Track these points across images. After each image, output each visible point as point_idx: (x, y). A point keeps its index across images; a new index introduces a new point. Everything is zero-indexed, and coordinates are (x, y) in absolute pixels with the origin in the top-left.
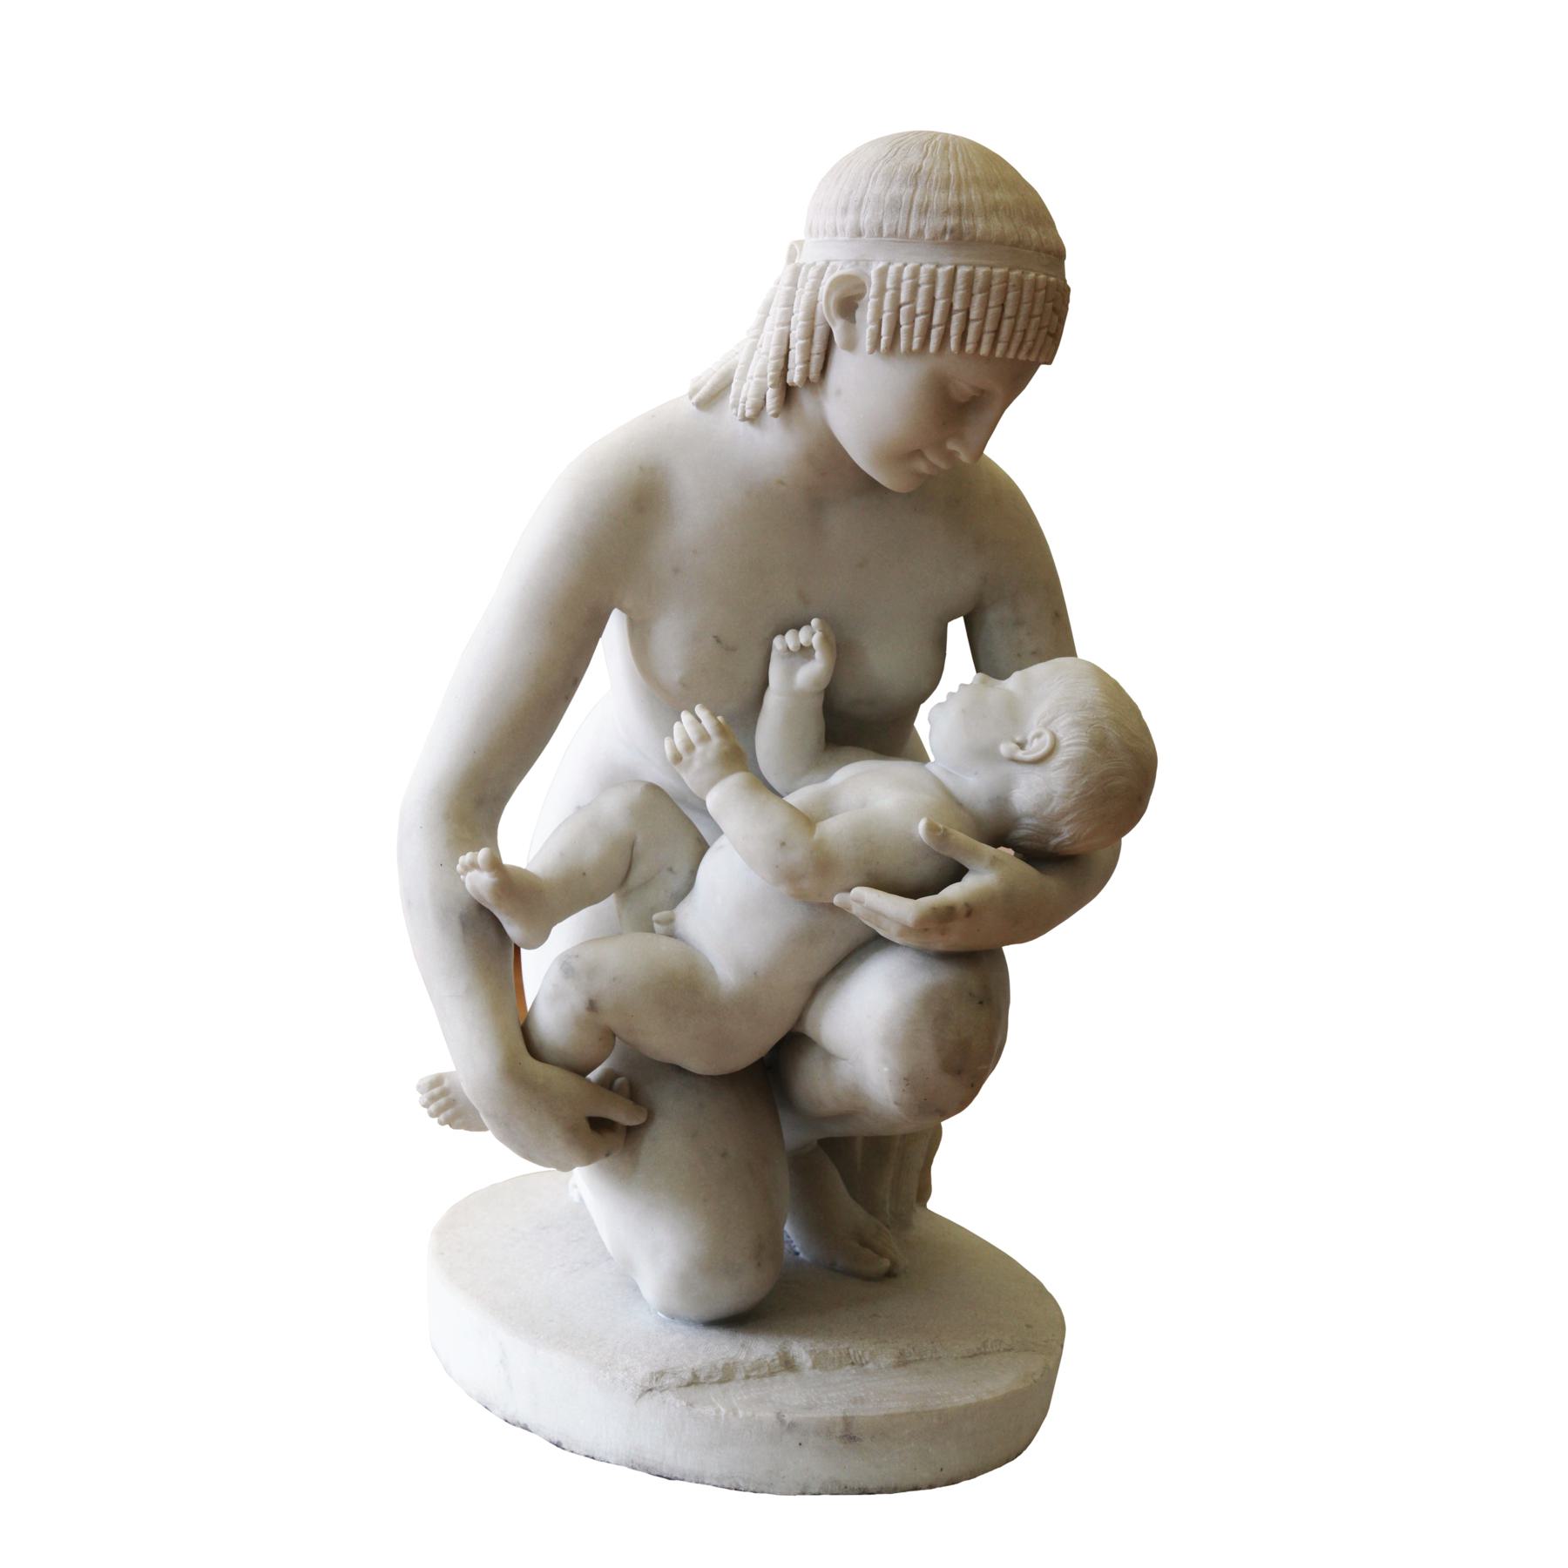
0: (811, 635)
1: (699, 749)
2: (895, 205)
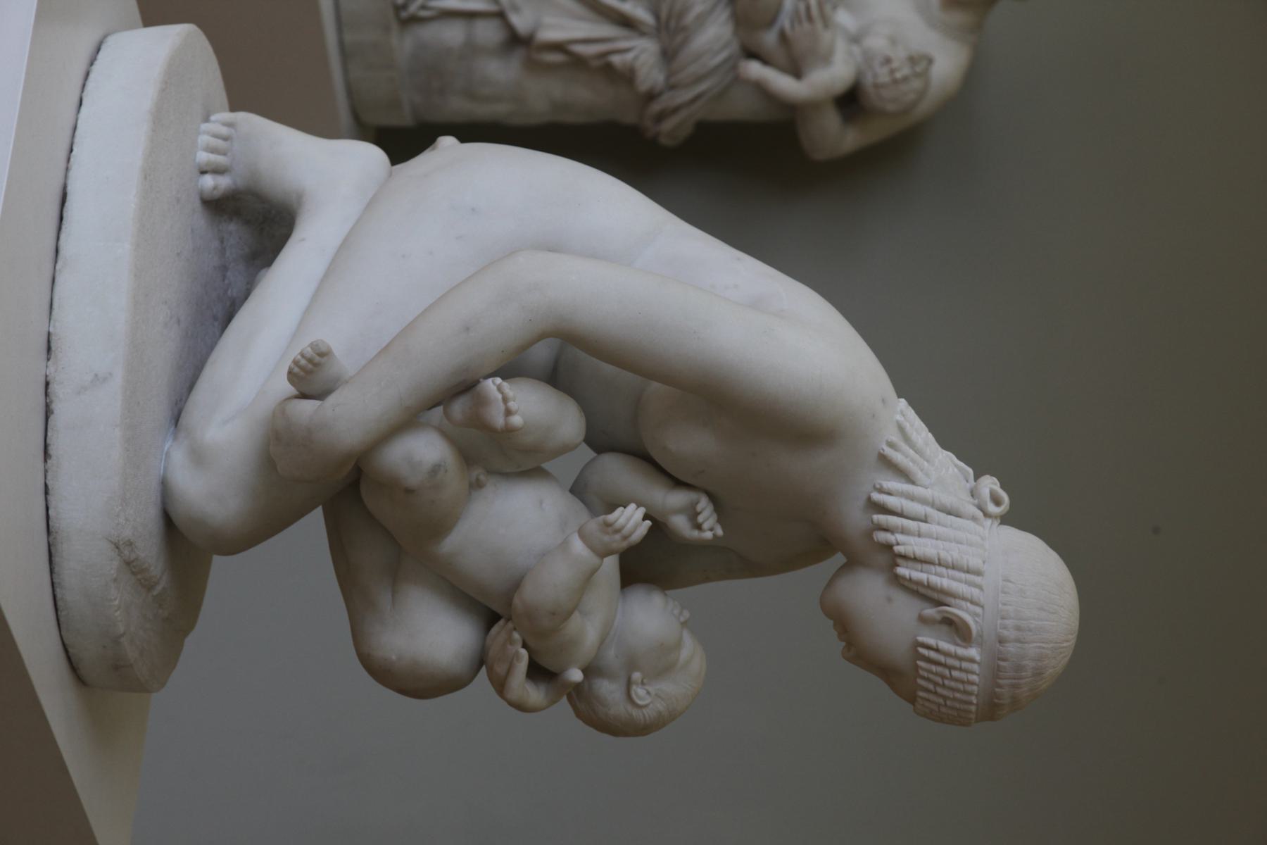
0: (710, 528)
1: (617, 537)
2: (1019, 668)
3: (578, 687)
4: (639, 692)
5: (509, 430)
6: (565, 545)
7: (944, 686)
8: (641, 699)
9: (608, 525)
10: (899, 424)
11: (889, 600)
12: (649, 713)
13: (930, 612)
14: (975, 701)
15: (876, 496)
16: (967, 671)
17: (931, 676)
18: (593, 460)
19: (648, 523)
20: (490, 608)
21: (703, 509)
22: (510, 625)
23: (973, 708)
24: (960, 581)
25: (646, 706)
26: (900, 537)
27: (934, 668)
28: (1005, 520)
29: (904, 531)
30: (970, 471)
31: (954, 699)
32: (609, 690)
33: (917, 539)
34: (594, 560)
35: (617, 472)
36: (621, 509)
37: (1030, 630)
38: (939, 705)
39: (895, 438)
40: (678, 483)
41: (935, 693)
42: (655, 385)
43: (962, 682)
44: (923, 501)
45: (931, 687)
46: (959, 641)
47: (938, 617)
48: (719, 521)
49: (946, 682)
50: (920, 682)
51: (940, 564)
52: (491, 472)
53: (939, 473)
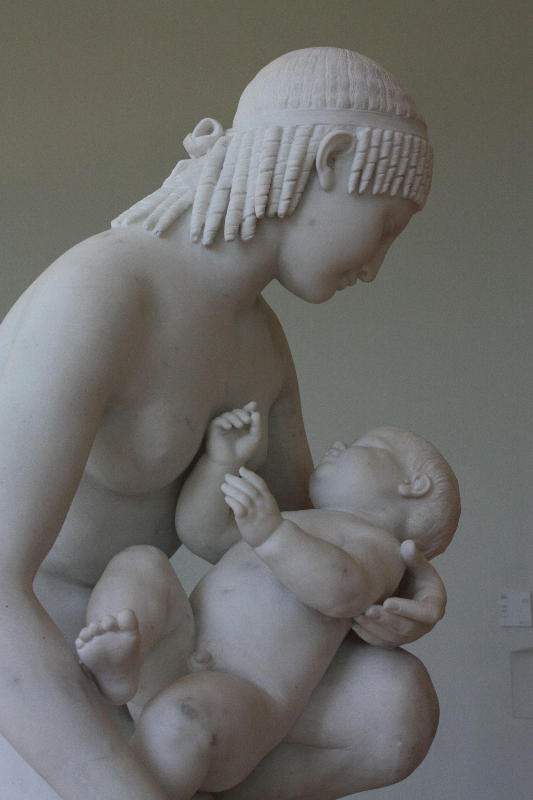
0: (248, 414)
1: (258, 503)
3: (420, 548)
4: (417, 487)
5: (134, 626)
6: (270, 562)
7: (397, 166)
8: (424, 486)
9: (245, 513)
10: (134, 224)
11: (312, 223)
12: (438, 478)
13: (322, 178)
14: (410, 136)
15: (206, 239)
16: (381, 141)
17: (388, 179)
18: (185, 545)
19: (242, 471)
20: (345, 641)
21: (229, 422)
22: (359, 619)
23: (416, 139)
24: (289, 149)
25: (431, 480)
26: (247, 211)
27: (379, 176)
28: (227, 123)
29: (241, 209)
30: (180, 163)
31: (409, 157)
32: (418, 517)
33: (248, 195)
34: (285, 526)
35: (193, 516)
36: (227, 500)
37: (335, 78)
38: (416, 175)
39: (145, 223)
40: (203, 450)
41: (404, 176)
42: (92, 467)
43: (392, 146)
44: (209, 193)
45: (398, 181)
46: (351, 150)
47: (327, 170)
48: (241, 407)
49: (393, 163)
50: (394, 191)
51: (273, 169)
52: (195, 649)
53: (184, 183)
